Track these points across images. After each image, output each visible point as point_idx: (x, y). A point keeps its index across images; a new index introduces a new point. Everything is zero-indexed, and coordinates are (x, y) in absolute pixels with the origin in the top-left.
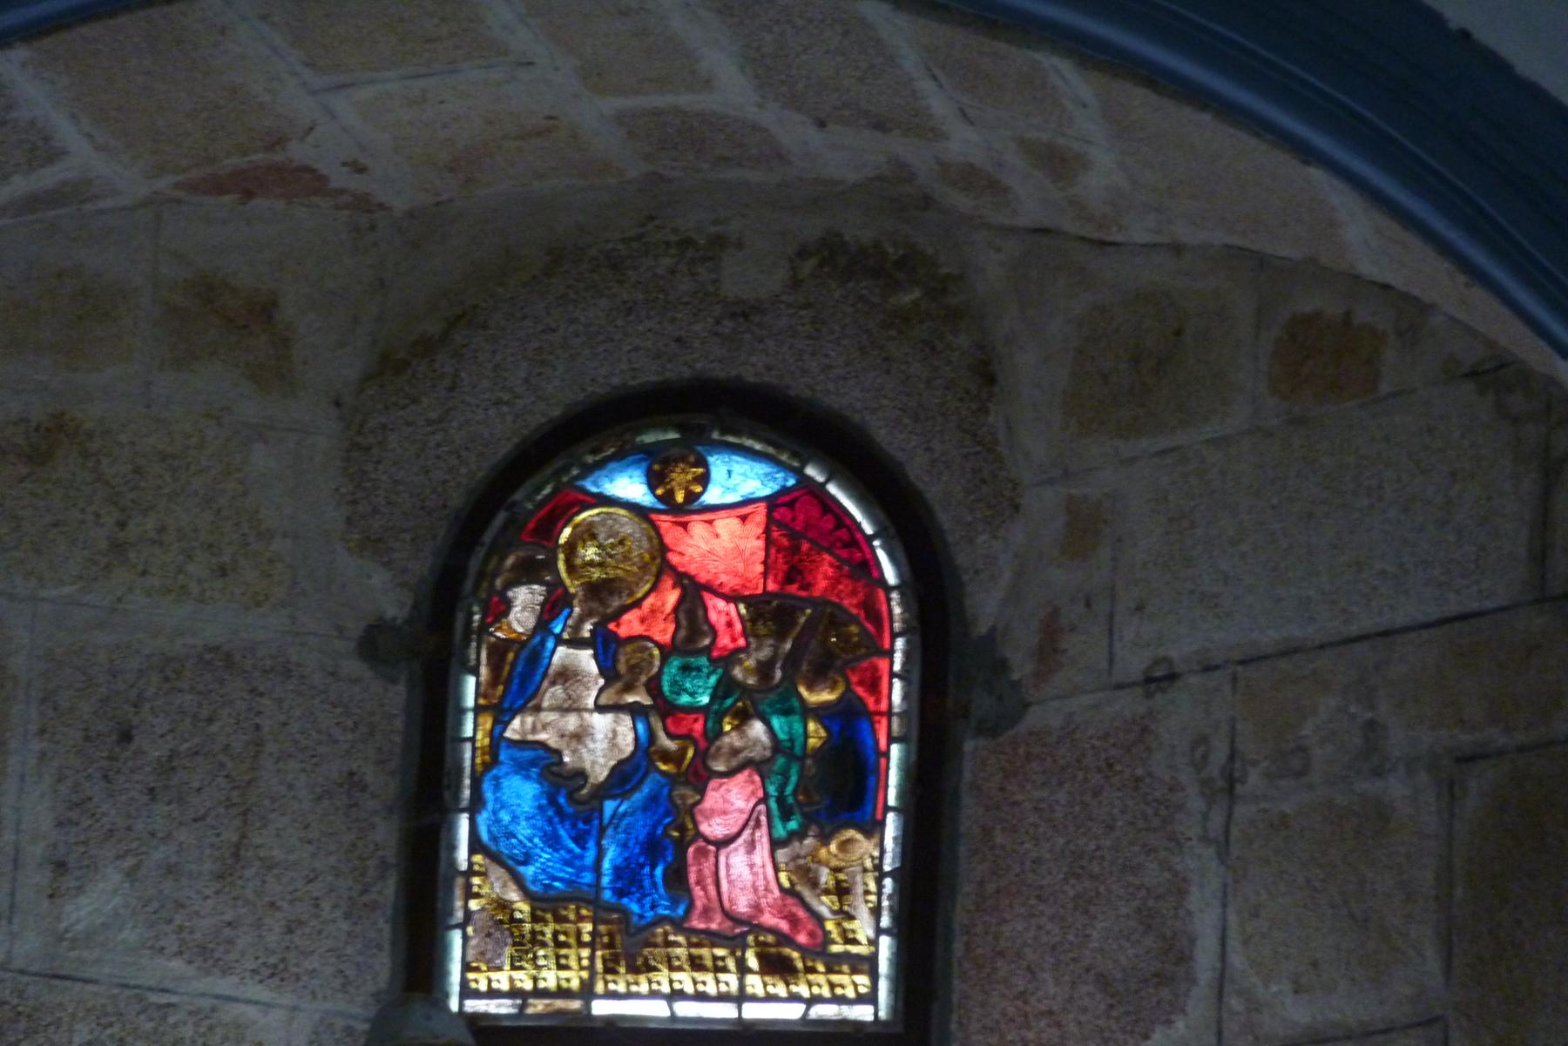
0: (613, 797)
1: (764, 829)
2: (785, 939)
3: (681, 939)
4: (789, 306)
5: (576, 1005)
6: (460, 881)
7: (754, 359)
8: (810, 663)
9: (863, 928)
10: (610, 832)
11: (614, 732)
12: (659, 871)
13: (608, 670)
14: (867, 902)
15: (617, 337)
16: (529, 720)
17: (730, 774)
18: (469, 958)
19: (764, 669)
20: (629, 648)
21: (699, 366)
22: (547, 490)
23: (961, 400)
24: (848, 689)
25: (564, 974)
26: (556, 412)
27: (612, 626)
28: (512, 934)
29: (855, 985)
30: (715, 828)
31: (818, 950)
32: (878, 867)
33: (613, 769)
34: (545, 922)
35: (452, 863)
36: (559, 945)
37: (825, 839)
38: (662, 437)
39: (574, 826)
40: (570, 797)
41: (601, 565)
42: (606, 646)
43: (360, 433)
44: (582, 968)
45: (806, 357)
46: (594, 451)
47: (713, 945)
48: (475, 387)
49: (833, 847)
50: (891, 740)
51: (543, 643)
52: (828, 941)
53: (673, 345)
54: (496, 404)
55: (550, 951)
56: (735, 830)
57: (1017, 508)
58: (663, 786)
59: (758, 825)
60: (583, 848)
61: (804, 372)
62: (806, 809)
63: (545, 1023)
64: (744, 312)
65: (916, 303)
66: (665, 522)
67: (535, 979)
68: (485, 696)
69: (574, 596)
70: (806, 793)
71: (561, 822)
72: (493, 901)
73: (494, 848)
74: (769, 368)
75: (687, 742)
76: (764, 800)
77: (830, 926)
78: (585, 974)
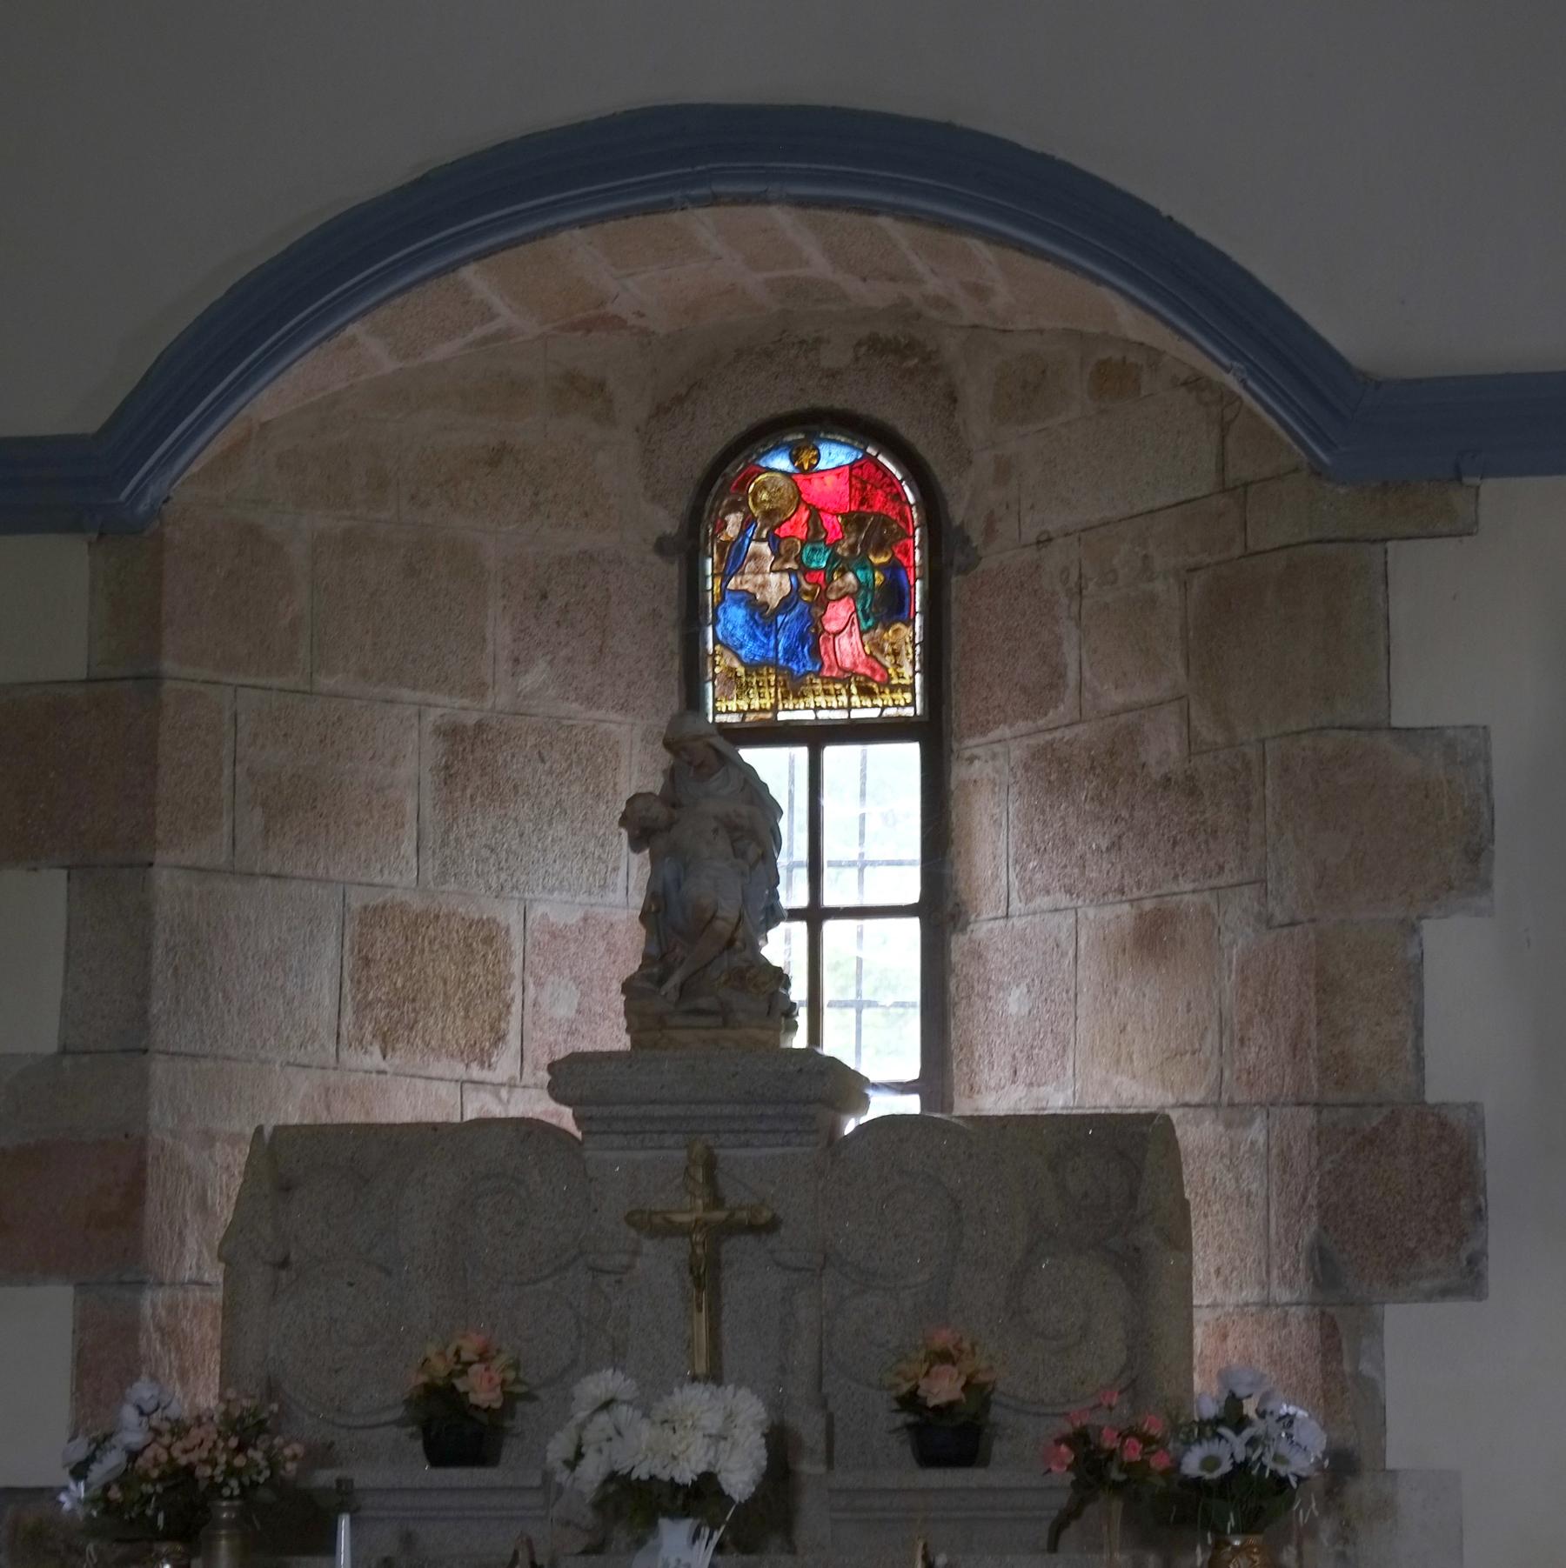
2: (868, 679)
5: (769, 715)
9: (907, 671)
13: (776, 554)
17: (839, 599)
19: (852, 548)
30: (832, 627)
37: (886, 629)
42: (774, 541)
52: (890, 678)
58: (806, 607)
64: (833, 374)
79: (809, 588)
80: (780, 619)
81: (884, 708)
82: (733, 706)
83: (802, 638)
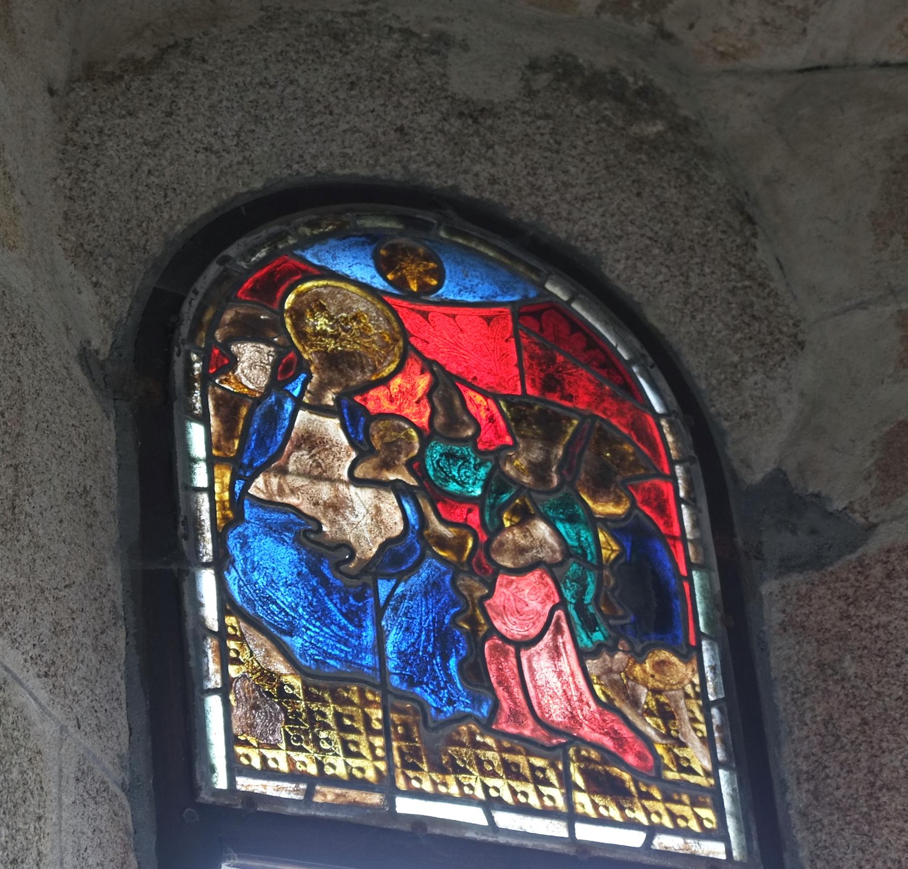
0: (388, 577)
1: (567, 634)
2: (609, 757)
3: (489, 741)
4: (524, 113)
5: (375, 799)
6: (210, 645)
7: (477, 168)
8: (587, 473)
9: (699, 759)
10: (388, 612)
11: (378, 510)
12: (452, 663)
13: (363, 447)
14: (695, 730)
15: (336, 111)
16: (274, 481)
17: (520, 571)
18: (236, 729)
19: (539, 470)
20: (381, 425)
21: (413, 167)
22: (262, 254)
23: (724, 232)
24: (633, 505)
25: (354, 762)
26: (258, 185)
27: (358, 399)
28: (284, 710)
29: (699, 819)
30: (512, 628)
31: (653, 773)
32: (702, 694)
33: (382, 547)
34: (325, 703)
35: (201, 621)
36: (342, 728)
37: (639, 657)
38: (380, 223)
39: (344, 600)
40: (337, 566)
41: (335, 337)
42: (355, 420)
43: (73, 130)
44: (376, 758)
45: (541, 171)
46: (311, 225)
47: (529, 754)
48: (190, 120)
49: (648, 666)
50: (690, 566)
51: (280, 404)
52: (660, 767)
53: (392, 135)
54: (206, 149)
55: (334, 735)
56: (534, 632)
57: (801, 345)
58: (446, 573)
59: (559, 630)
60: (360, 626)
61: (536, 189)
62: (611, 622)
63: (340, 815)
64: (475, 113)
65: (659, 134)
66: (403, 306)
67: (320, 765)
68: (218, 448)
69: (309, 362)
70: (608, 603)
71: (328, 594)
72: (254, 671)
73: (251, 612)
74: (493, 181)
75: (464, 531)
76: (562, 603)
77: (660, 750)
78: (382, 766)
79: (448, 532)
80: (384, 588)
81: (652, 830)
82: (279, 759)
83: (443, 639)
